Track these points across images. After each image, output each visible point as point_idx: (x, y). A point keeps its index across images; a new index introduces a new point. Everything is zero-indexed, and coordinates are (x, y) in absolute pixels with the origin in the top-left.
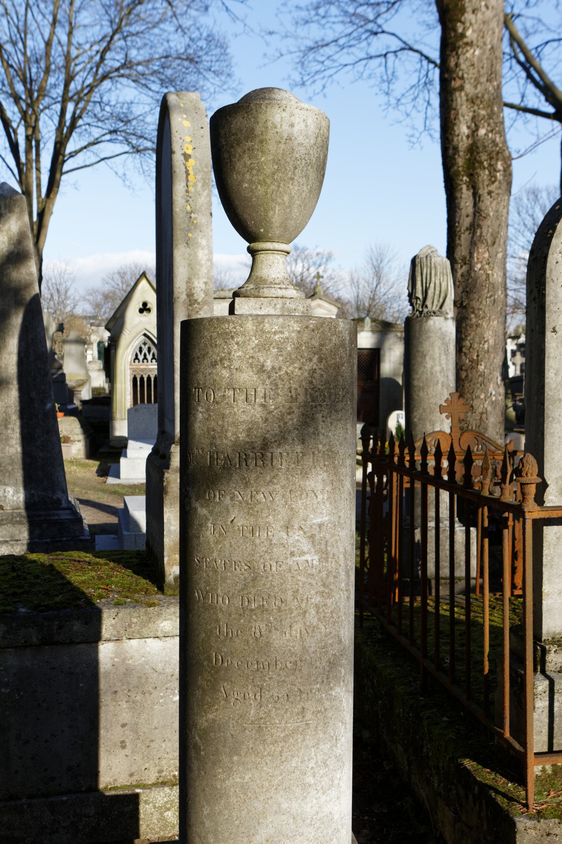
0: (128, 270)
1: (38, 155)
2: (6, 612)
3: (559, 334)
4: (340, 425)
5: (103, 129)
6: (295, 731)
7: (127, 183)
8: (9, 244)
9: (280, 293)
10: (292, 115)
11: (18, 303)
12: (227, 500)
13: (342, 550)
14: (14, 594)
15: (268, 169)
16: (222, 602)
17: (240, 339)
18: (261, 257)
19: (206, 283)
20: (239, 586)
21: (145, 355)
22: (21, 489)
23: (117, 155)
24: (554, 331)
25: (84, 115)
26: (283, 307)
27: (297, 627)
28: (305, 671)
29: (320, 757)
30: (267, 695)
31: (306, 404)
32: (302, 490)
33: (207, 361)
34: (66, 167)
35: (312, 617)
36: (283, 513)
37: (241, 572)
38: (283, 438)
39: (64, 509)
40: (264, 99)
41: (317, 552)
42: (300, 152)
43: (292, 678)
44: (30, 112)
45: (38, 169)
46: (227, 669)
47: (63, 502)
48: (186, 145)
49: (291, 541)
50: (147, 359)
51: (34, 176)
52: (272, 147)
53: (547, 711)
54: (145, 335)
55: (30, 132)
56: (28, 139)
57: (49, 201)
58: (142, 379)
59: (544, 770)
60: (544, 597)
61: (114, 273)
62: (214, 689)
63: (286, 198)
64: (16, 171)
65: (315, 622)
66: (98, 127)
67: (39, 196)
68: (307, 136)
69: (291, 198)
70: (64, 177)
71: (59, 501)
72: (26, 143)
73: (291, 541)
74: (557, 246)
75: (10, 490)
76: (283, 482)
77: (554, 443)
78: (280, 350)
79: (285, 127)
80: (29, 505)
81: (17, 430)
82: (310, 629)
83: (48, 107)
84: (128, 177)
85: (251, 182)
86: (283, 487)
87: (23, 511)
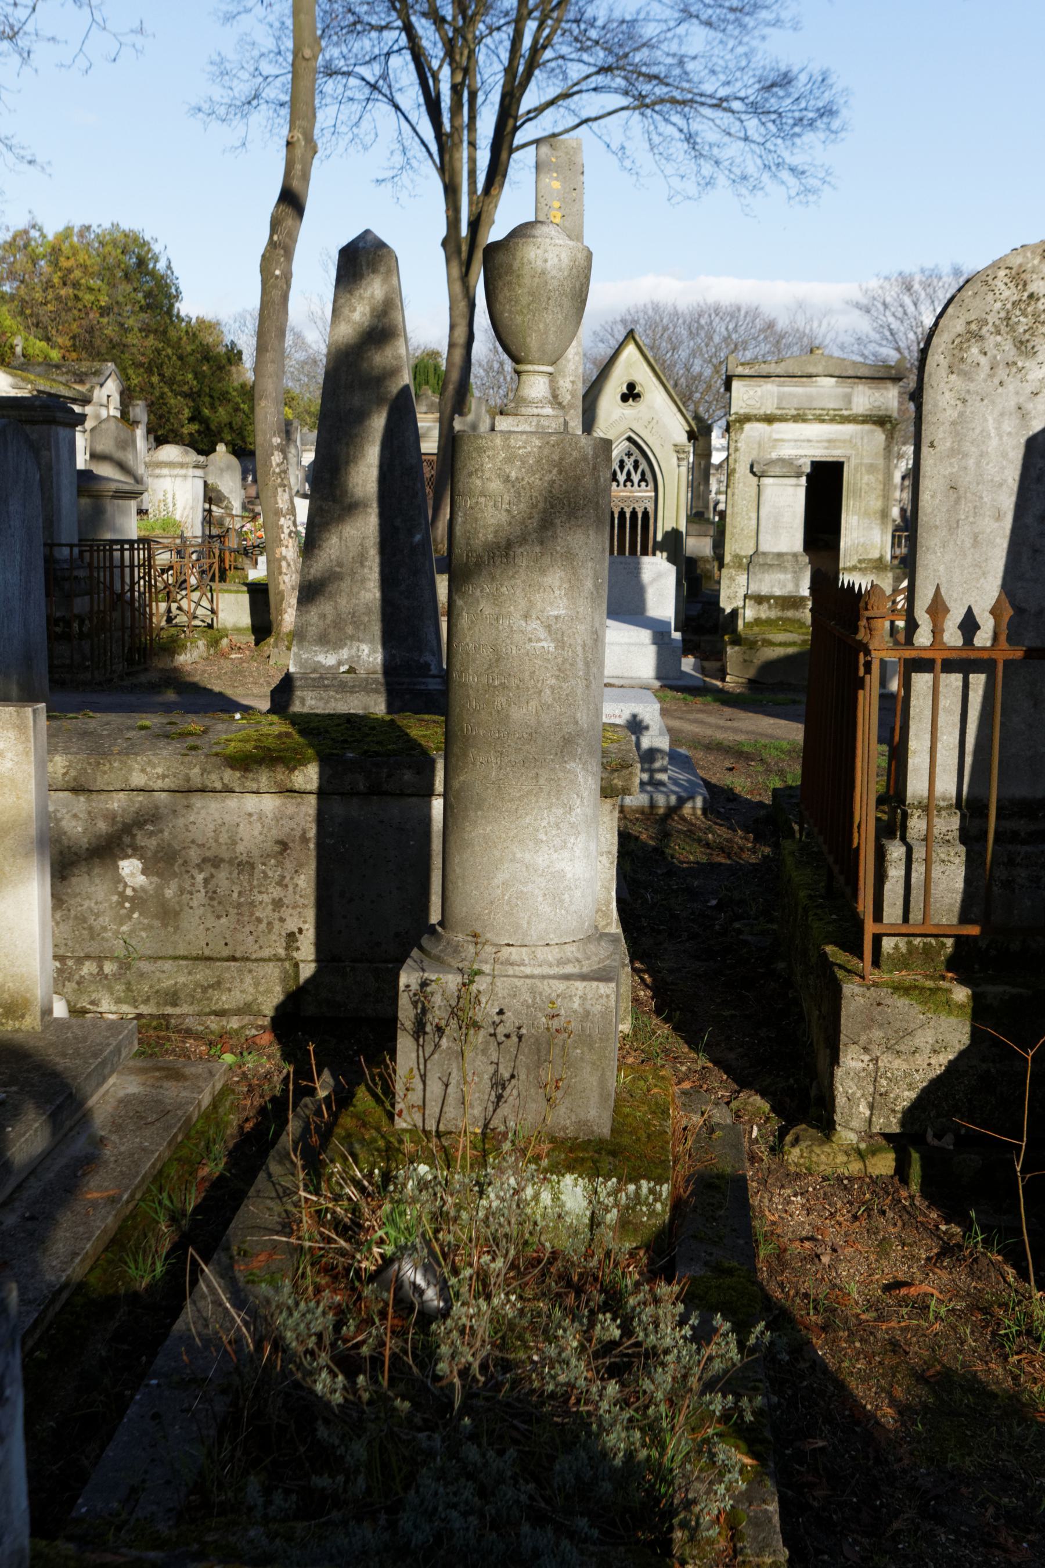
0: (641, 315)
1: (472, 118)
2: (333, 754)
3: (938, 449)
4: (579, 531)
5: (589, 64)
6: (530, 792)
7: (627, 163)
8: (372, 316)
9: (536, 411)
10: (546, 251)
11: (380, 401)
12: (478, 593)
13: (580, 641)
14: (345, 741)
15: (525, 300)
16: (472, 679)
17: (490, 453)
18: (524, 377)
19: (573, 382)
20: (486, 666)
21: (629, 474)
22: (379, 648)
23: (610, 114)
24: (932, 445)
25: (556, 39)
26: (537, 425)
27: (533, 704)
28: (540, 741)
29: (552, 820)
30: (506, 760)
31: (545, 511)
32: (540, 585)
33: (465, 472)
34: (520, 138)
35: (547, 696)
36: (523, 604)
37: (487, 653)
38: (524, 539)
39: (434, 676)
40: (525, 236)
41: (553, 640)
42: (554, 284)
43: (527, 747)
44: (460, 42)
45: (472, 144)
46: (475, 737)
47: (433, 667)
48: (553, 213)
49: (529, 628)
50: (632, 481)
51: (465, 155)
52: (527, 281)
53: (902, 881)
54: (629, 439)
55: (459, 78)
56: (456, 90)
57: (487, 201)
58: (634, 513)
59: (896, 947)
60: (910, 755)
61: (615, 323)
62: (465, 755)
63: (541, 326)
64: (434, 148)
65: (550, 701)
66: (580, 61)
67: (472, 190)
68: (560, 270)
69: (546, 325)
70: (515, 156)
71: (427, 666)
72: (452, 100)
73: (529, 628)
74: (938, 345)
75: (365, 648)
76: (524, 577)
77: (927, 578)
78: (523, 463)
79: (539, 263)
80: (389, 668)
81: (376, 569)
82: (546, 707)
83: (491, 30)
84: (628, 152)
85: (510, 312)
86: (523, 582)
87: (380, 677)
